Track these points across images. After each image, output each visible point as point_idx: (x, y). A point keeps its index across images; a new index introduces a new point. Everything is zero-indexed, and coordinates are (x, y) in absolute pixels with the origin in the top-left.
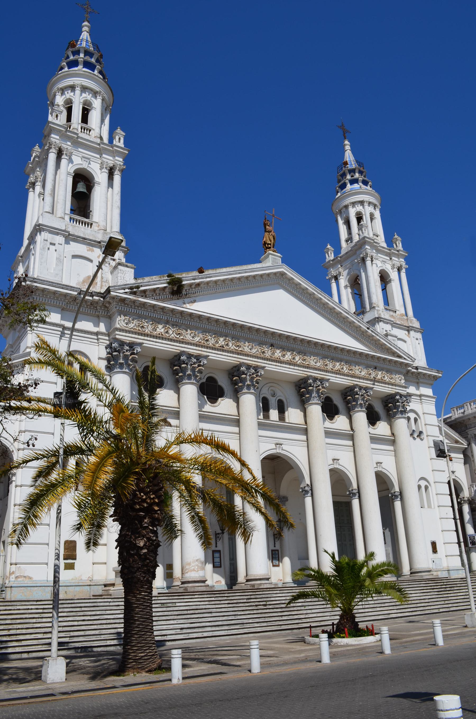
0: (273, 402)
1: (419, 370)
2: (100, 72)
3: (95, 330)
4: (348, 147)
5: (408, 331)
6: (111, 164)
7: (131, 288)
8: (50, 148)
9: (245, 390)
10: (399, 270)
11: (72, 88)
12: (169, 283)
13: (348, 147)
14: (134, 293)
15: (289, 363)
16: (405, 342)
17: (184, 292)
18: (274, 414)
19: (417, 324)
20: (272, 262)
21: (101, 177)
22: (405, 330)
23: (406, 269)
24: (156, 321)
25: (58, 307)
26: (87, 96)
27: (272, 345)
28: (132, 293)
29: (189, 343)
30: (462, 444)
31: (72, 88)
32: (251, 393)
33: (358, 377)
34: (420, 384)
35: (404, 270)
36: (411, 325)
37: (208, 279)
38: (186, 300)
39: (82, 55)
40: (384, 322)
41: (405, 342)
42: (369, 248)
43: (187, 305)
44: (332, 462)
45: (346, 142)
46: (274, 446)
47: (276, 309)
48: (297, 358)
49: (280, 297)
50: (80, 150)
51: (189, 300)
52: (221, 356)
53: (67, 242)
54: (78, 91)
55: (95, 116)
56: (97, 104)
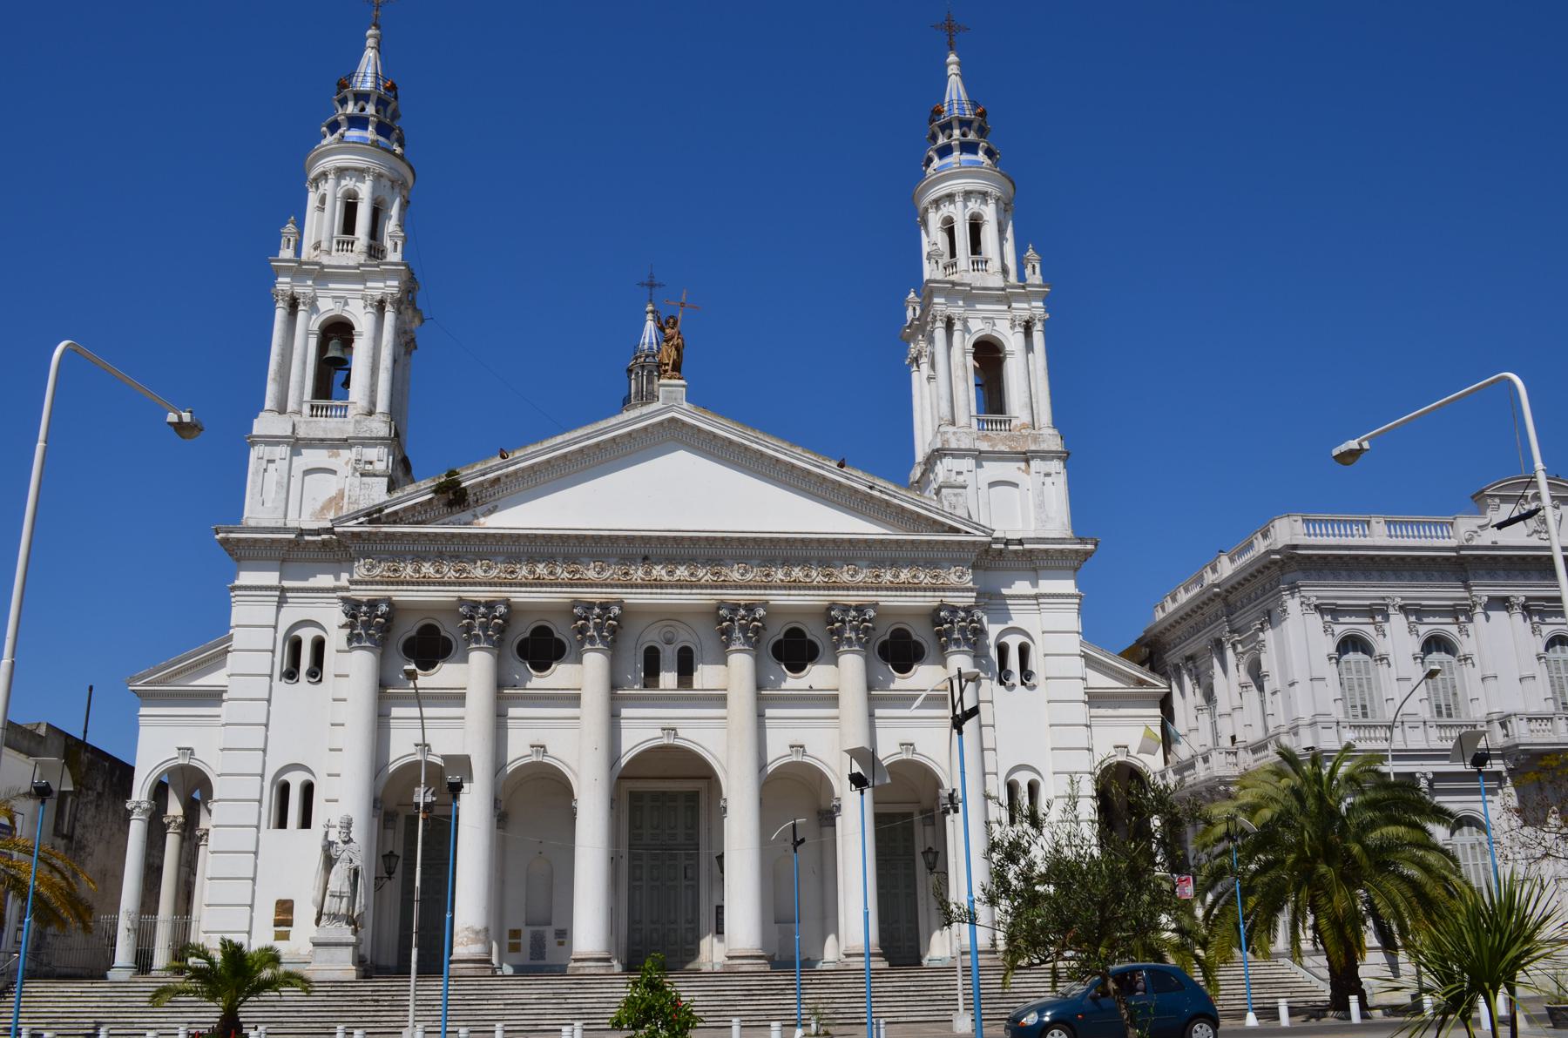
0: (669, 655)
1: (1027, 546)
2: (990, 153)
3: (1034, 591)
4: (953, 69)
5: (1027, 461)
6: (1026, 315)
7: (368, 514)
8: (934, 321)
9: (587, 646)
10: (1028, 328)
11: (950, 197)
12: (435, 492)
13: (953, 69)
14: (378, 521)
15: (680, 585)
16: (1016, 485)
17: (471, 498)
18: (668, 679)
19: (1053, 442)
20: (671, 399)
21: (1013, 341)
22: (1018, 460)
23: (1046, 323)
24: (419, 558)
25: (1069, 568)
26: (974, 206)
27: (645, 559)
28: (370, 522)
29: (482, 585)
30: (1155, 686)
31: (950, 197)
32: (853, 652)
33: (851, 589)
34: (1041, 572)
35: (1038, 326)
36: (1033, 448)
37: (511, 469)
38: (479, 510)
39: (957, 133)
40: (954, 456)
41: (1016, 485)
42: (942, 300)
43: (482, 520)
44: (788, 751)
45: (952, 58)
46: (659, 733)
47: (683, 492)
48: (701, 573)
49: (681, 464)
50: (979, 307)
51: (485, 508)
52: (538, 594)
53: (979, 466)
54: (959, 199)
55: (989, 234)
56: (989, 213)
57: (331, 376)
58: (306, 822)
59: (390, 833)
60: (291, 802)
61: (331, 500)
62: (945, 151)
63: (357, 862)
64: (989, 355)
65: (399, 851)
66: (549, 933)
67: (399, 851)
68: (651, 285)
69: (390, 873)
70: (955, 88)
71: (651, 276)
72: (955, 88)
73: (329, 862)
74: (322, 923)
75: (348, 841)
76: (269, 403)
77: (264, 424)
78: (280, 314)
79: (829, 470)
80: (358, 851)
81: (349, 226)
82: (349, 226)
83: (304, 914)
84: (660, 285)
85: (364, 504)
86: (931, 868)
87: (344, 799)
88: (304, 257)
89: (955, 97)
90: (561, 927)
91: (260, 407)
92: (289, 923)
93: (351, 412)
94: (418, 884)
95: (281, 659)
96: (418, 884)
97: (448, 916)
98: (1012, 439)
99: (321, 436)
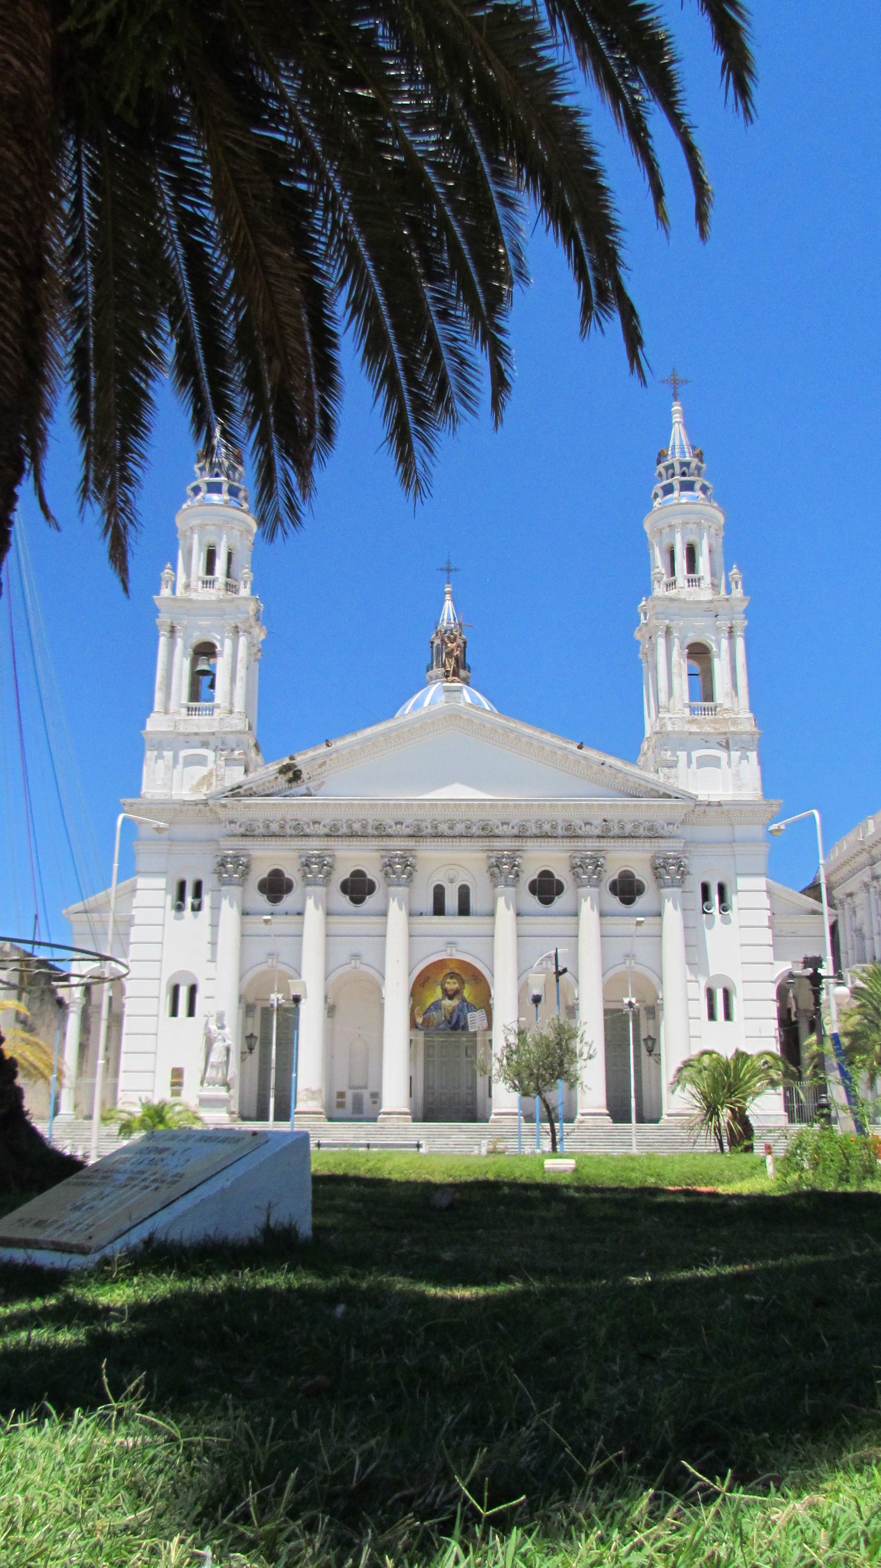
2: (704, 489)
4: (677, 418)
13: (677, 418)
36: (732, 729)
57: (201, 684)
58: (191, 1013)
59: (250, 1020)
60: (183, 998)
61: (205, 777)
62: (668, 490)
63: (228, 1042)
64: (699, 653)
65: (257, 1033)
66: (366, 1094)
67: (257, 1033)
68: (449, 570)
69: (251, 1049)
70: (678, 435)
71: (449, 563)
72: (678, 435)
73: (209, 1043)
74: (206, 1085)
75: (222, 1027)
76: (157, 706)
77: (155, 724)
78: (163, 641)
79: (249, 1279)
80: (230, 1036)
81: (210, 568)
82: (210, 568)
83: (191, 1080)
84: (456, 570)
85: (229, 783)
86: (650, 1051)
87: (220, 998)
88: (178, 594)
89: (677, 443)
90: (375, 1090)
91: (150, 709)
92: (180, 1084)
93: (217, 585)
94: (274, 1056)
95: (170, 900)
96: (274, 1056)
97: (294, 1075)
98: (716, 722)
99: (195, 730)
